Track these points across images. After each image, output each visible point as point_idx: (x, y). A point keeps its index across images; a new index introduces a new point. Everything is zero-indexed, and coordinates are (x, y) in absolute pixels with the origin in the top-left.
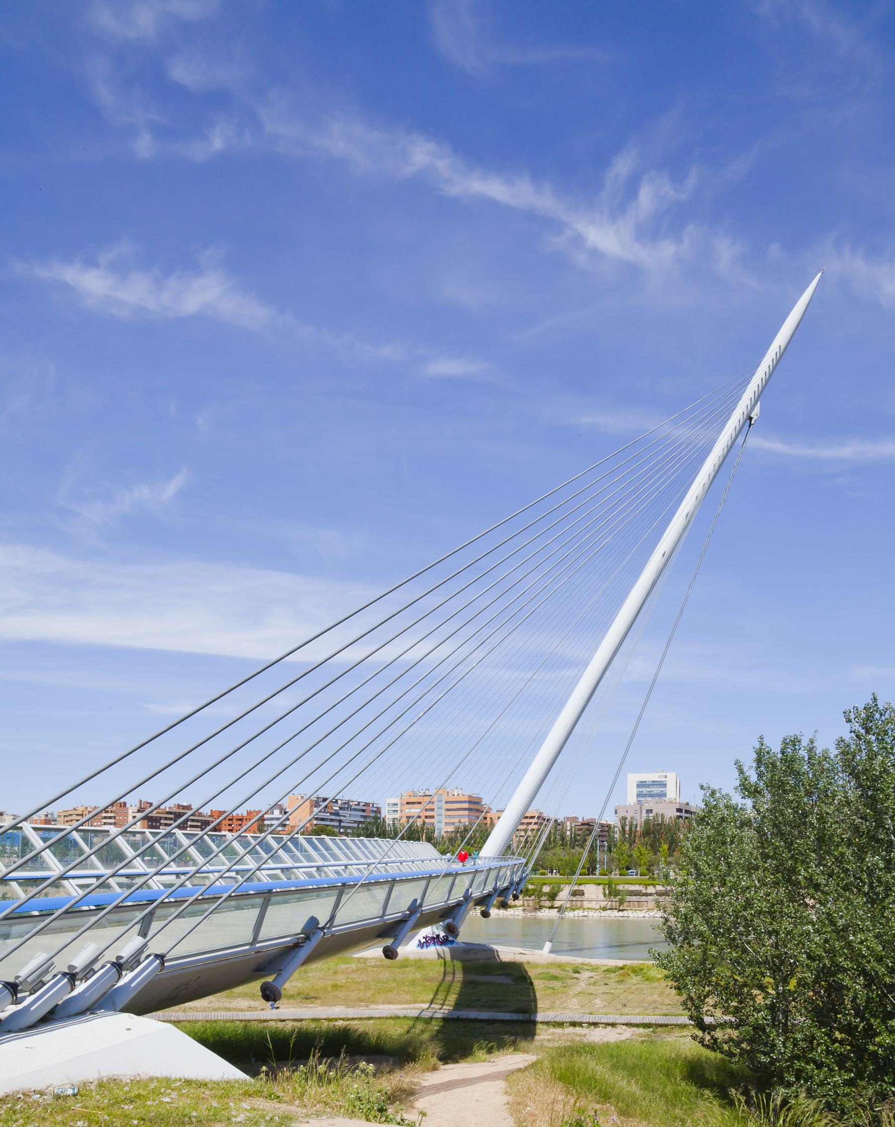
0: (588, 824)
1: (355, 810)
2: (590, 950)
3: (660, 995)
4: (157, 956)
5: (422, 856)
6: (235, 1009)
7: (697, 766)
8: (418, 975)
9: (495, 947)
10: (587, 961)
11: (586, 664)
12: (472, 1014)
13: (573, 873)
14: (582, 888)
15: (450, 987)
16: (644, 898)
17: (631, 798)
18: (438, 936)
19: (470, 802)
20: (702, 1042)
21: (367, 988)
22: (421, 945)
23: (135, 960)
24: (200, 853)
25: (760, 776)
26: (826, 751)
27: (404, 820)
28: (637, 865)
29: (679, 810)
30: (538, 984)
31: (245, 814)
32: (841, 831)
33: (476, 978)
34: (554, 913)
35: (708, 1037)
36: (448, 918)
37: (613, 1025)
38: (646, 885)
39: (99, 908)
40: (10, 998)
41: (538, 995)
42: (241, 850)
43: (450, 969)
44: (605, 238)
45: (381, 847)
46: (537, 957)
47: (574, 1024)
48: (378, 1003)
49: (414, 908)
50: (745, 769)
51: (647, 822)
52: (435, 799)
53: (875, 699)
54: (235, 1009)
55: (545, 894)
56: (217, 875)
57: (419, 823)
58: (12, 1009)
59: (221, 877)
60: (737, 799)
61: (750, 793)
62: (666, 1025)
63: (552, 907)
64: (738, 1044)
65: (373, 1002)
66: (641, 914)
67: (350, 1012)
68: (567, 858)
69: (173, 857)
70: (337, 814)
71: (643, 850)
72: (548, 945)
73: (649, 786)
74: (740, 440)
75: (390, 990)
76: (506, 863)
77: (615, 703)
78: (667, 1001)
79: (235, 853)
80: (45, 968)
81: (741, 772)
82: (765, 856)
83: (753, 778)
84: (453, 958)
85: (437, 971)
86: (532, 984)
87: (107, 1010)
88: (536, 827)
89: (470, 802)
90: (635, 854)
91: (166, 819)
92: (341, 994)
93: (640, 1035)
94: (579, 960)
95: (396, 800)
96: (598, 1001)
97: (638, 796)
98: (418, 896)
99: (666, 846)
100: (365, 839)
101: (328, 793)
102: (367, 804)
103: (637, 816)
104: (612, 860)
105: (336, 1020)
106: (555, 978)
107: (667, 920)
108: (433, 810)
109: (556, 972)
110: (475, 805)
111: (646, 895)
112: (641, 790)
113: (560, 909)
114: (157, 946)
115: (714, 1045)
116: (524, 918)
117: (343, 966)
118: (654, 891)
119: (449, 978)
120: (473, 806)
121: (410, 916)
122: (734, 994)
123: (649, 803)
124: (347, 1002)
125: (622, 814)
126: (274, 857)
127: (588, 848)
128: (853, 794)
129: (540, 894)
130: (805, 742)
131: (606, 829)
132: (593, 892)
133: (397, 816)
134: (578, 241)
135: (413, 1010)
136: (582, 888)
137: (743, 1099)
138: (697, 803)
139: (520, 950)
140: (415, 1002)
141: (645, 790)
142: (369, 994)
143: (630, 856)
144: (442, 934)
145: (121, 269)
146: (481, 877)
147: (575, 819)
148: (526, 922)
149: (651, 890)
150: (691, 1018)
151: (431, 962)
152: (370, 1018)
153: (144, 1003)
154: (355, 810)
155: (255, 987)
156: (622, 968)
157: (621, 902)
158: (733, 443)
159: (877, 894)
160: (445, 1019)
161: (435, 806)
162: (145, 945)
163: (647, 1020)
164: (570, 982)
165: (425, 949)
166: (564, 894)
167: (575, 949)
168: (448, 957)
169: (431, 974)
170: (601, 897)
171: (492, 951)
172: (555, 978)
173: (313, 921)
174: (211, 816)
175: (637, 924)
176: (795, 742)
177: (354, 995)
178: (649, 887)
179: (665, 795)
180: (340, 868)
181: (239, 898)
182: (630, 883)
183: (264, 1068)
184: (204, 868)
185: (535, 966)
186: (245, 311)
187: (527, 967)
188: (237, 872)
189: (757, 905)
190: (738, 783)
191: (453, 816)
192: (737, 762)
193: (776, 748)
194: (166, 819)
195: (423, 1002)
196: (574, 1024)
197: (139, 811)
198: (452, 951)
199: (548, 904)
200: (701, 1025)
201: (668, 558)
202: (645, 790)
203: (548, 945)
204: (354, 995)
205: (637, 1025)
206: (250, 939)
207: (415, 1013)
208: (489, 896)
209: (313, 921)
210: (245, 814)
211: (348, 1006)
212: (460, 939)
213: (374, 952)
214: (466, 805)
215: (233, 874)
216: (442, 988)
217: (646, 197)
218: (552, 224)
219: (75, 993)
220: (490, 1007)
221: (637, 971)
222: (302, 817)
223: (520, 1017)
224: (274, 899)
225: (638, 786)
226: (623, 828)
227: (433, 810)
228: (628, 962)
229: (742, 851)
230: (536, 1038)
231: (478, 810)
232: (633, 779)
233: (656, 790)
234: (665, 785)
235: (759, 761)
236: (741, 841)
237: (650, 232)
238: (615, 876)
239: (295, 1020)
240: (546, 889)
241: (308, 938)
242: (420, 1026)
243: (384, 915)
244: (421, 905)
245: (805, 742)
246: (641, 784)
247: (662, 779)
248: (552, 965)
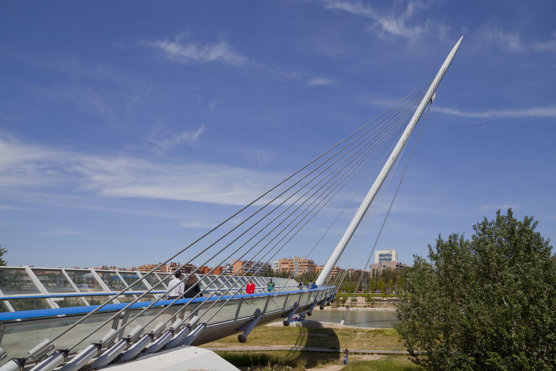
0: (358, 272)
2: (359, 323)
3: (391, 342)
4: (203, 324)
5: (291, 285)
6: (215, 347)
7: (410, 248)
8: (290, 333)
9: (321, 322)
10: (359, 328)
11: (359, 205)
12: (313, 349)
13: (353, 292)
14: (356, 298)
15: (303, 338)
16: (382, 302)
17: (377, 261)
19: (309, 263)
20: (412, 361)
21: (268, 339)
23: (195, 325)
25: (439, 251)
26: (468, 240)
27: (281, 270)
28: (379, 289)
29: (397, 266)
30: (340, 337)
32: (473, 274)
33: (314, 334)
34: (344, 309)
35: (415, 359)
36: (308, 309)
37: (372, 354)
38: (383, 297)
39: (166, 306)
40: (151, 340)
41: (340, 342)
42: (222, 283)
43: (302, 331)
44: (391, 26)
45: (264, 281)
46: (339, 326)
47: (355, 353)
48: (273, 345)
49: (296, 305)
50: (432, 248)
51: (384, 271)
52: (294, 261)
53: (486, 219)
54: (215, 347)
55: (341, 300)
56: (213, 292)
57: (287, 271)
58: (150, 344)
59: (116, 298)
60: (428, 261)
61: (434, 258)
62: (394, 354)
63: (344, 306)
64: (427, 362)
65: (271, 344)
66: (381, 309)
67: (262, 348)
68: (350, 285)
69: (131, 285)
71: (382, 283)
72: (343, 321)
75: (279, 339)
76: (329, 288)
77: (376, 220)
78: (394, 344)
79: (220, 283)
80: (163, 328)
81: (431, 249)
82: (441, 285)
83: (436, 252)
84: (303, 326)
85: (297, 332)
86: (337, 337)
87: (186, 345)
88: (336, 273)
89: (309, 263)
90: (379, 284)
92: (258, 341)
93: (383, 358)
94: (356, 328)
95: (278, 262)
96: (365, 344)
97: (379, 260)
98: (297, 300)
99: (392, 281)
100: (263, 278)
101: (248, 258)
103: (379, 268)
104: (369, 287)
105: (257, 351)
106: (346, 335)
107: (398, 311)
109: (347, 332)
110: (311, 264)
111: (383, 301)
113: (347, 307)
114: (203, 321)
115: (417, 362)
116: (332, 310)
117: (258, 330)
119: (302, 335)
121: (294, 309)
122: (428, 340)
123: (385, 263)
124: (260, 344)
125: (373, 267)
126: (235, 285)
127: (359, 282)
128: (478, 258)
129: (339, 301)
130: (459, 237)
131: (366, 274)
132: (361, 300)
133: (278, 268)
134: (380, 27)
135: (288, 347)
136: (356, 298)
138: (410, 263)
139: (331, 323)
140: (289, 344)
141: (382, 258)
142: (269, 341)
143: (377, 285)
144: (298, 317)
145: (184, 43)
146: (320, 293)
147: (353, 270)
148: (332, 312)
149: (385, 299)
150: (408, 350)
151: (294, 328)
152: (271, 351)
153: (198, 342)
155: (235, 337)
156: (374, 331)
157: (373, 304)
158: (424, 111)
159: (491, 300)
160: (302, 351)
162: (199, 319)
163: (386, 352)
164: (353, 336)
166: (349, 301)
167: (353, 323)
168: (301, 326)
169: (295, 333)
170: (364, 302)
171: (319, 324)
172: (346, 335)
173: (258, 310)
175: (379, 312)
176: (455, 236)
177: (263, 341)
179: (391, 260)
180: (261, 290)
181: (232, 302)
182: (377, 297)
183: (249, 368)
184: (152, 291)
185: (338, 330)
186: (236, 59)
187: (334, 330)
188: (222, 291)
189: (439, 305)
190: (429, 254)
191: (302, 269)
192: (429, 246)
193: (445, 239)
195: (292, 344)
196: (355, 353)
198: (302, 323)
199: (342, 304)
200: (412, 354)
201: (395, 160)
202: (382, 258)
203: (343, 321)
204: (263, 341)
205: (382, 354)
206: (234, 317)
207: (289, 349)
208: (323, 301)
209: (258, 310)
211: (261, 346)
213: (279, 324)
214: (307, 264)
215: (220, 292)
216: (299, 339)
217: (410, 8)
218: (371, 21)
219: (173, 338)
220: (320, 346)
221: (381, 332)
222: (238, 268)
223: (333, 350)
224: (244, 302)
225: (380, 256)
226: (374, 273)
228: (377, 328)
229: (431, 283)
230: (340, 359)
232: (377, 253)
233: (387, 257)
234: (391, 256)
235: (438, 245)
236: (431, 278)
237: (410, 24)
238: (370, 293)
239: (240, 351)
240: (341, 298)
241: (256, 317)
242: (291, 354)
243: (284, 308)
244: (298, 304)
245: (459, 237)
246: (381, 255)
248: (345, 329)
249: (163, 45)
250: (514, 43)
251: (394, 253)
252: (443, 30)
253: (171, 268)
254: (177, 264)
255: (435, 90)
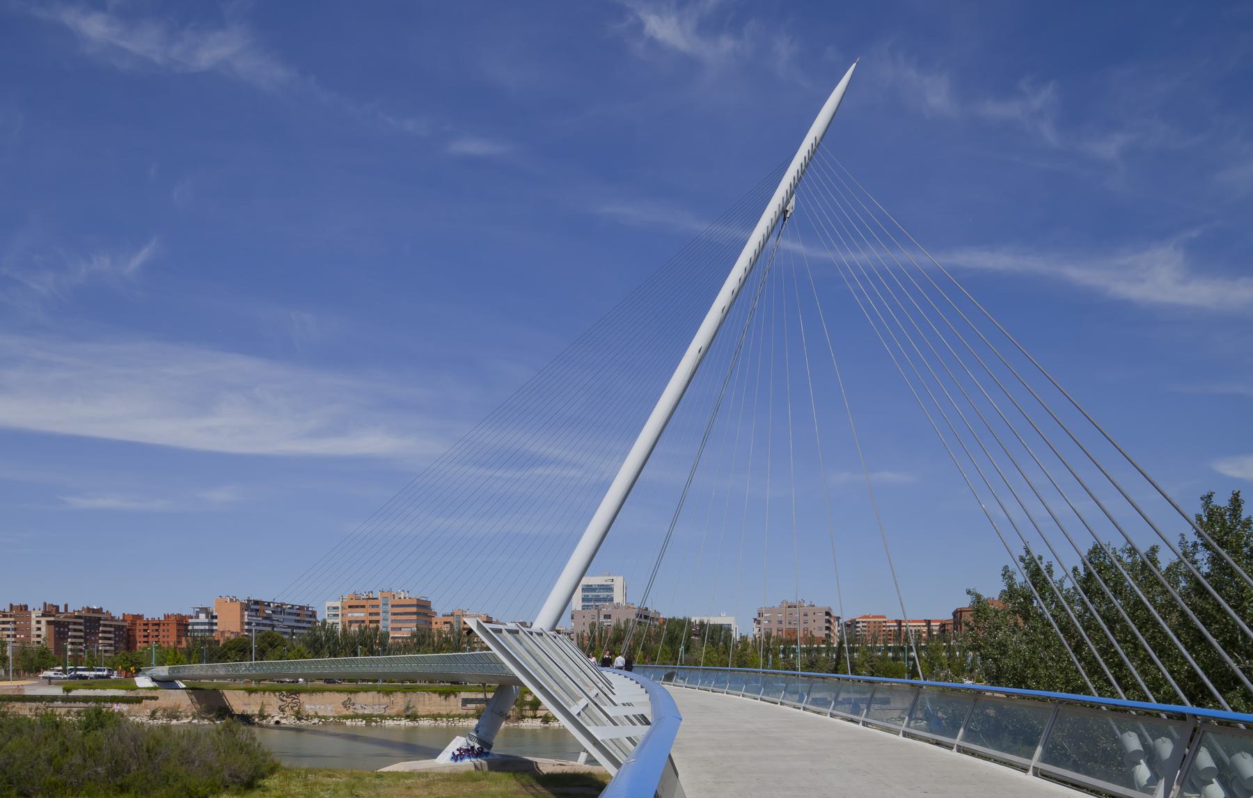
1: (290, 614)
18: (473, 748)
19: (418, 606)
22: (455, 758)
31: (162, 618)
34: (537, 723)
63: (535, 717)
70: (268, 618)
74: (772, 240)
89: (418, 606)
91: (75, 623)
95: (338, 604)
97: (584, 600)
102: (301, 608)
108: (378, 614)
120: (422, 611)
134: (639, 26)
141: (591, 594)
144: (477, 746)
154: (290, 614)
161: (380, 610)
165: (459, 762)
174: (124, 620)
179: (612, 600)
186: (264, 71)
194: (75, 623)
197: (43, 615)
199: (531, 713)
201: (705, 354)
202: (591, 594)
210: (162, 618)
212: (493, 751)
214: (414, 609)
227: (378, 614)
231: (426, 615)
233: (603, 594)
237: (709, 27)
249: (70, 17)
250: (936, 95)
251: (618, 583)
252: (784, 49)
253: (44, 620)
254: (62, 610)
255: (794, 189)
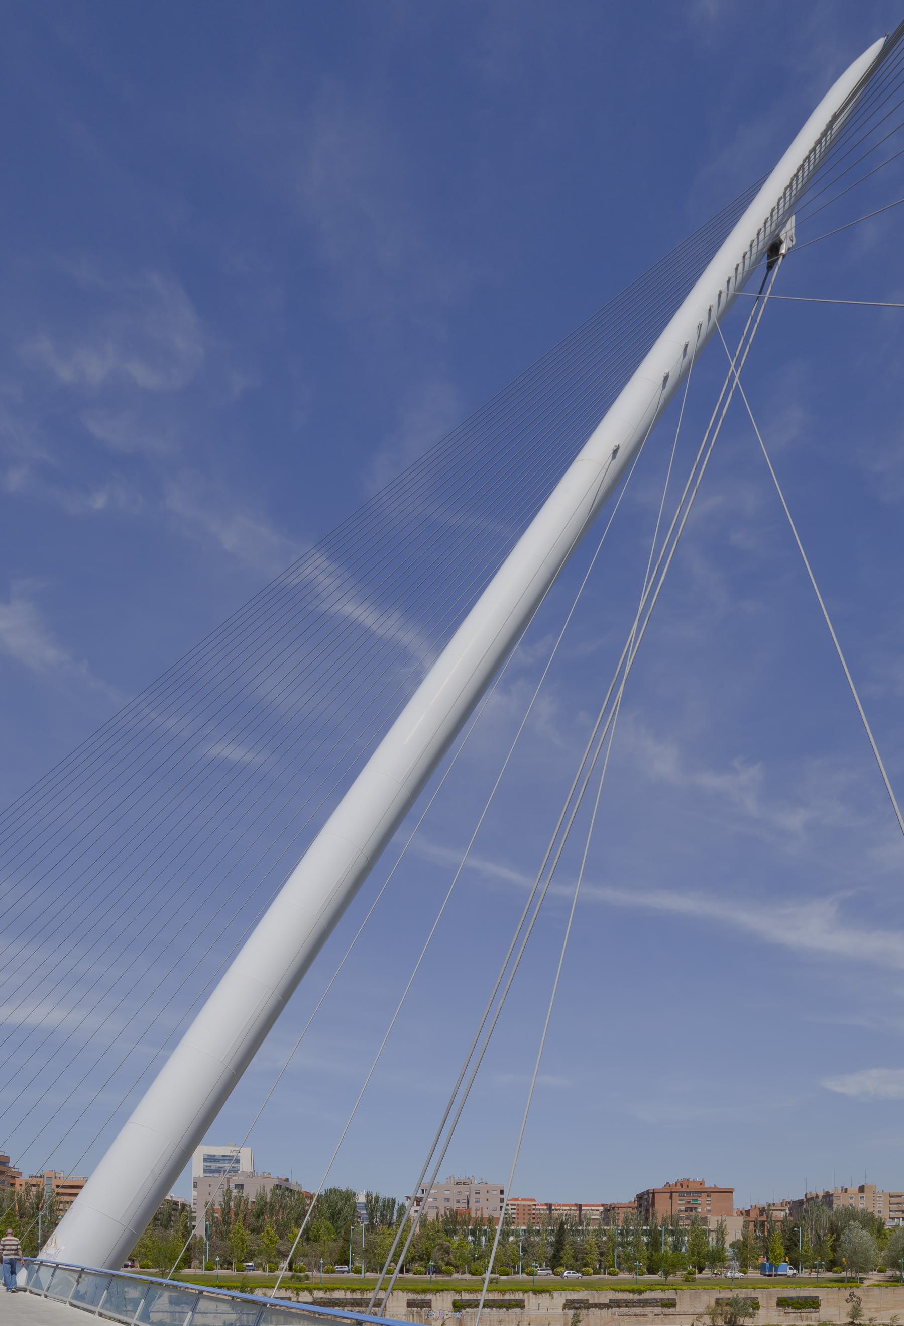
24: (806, 1298)
73: (218, 1160)
97: (205, 1171)
112: (209, 1164)
118: (310, 1299)
136: (429, 1297)
137: (896, 1220)
141: (214, 1165)
178: (302, 1294)
202: (214, 1165)
225: (205, 1160)
246: (209, 1158)
247: (234, 1154)
